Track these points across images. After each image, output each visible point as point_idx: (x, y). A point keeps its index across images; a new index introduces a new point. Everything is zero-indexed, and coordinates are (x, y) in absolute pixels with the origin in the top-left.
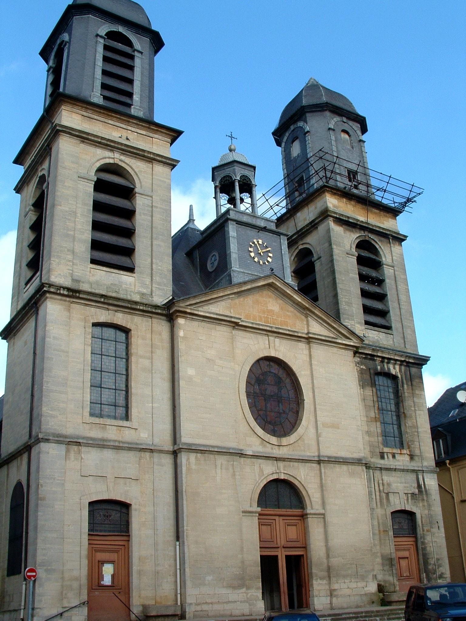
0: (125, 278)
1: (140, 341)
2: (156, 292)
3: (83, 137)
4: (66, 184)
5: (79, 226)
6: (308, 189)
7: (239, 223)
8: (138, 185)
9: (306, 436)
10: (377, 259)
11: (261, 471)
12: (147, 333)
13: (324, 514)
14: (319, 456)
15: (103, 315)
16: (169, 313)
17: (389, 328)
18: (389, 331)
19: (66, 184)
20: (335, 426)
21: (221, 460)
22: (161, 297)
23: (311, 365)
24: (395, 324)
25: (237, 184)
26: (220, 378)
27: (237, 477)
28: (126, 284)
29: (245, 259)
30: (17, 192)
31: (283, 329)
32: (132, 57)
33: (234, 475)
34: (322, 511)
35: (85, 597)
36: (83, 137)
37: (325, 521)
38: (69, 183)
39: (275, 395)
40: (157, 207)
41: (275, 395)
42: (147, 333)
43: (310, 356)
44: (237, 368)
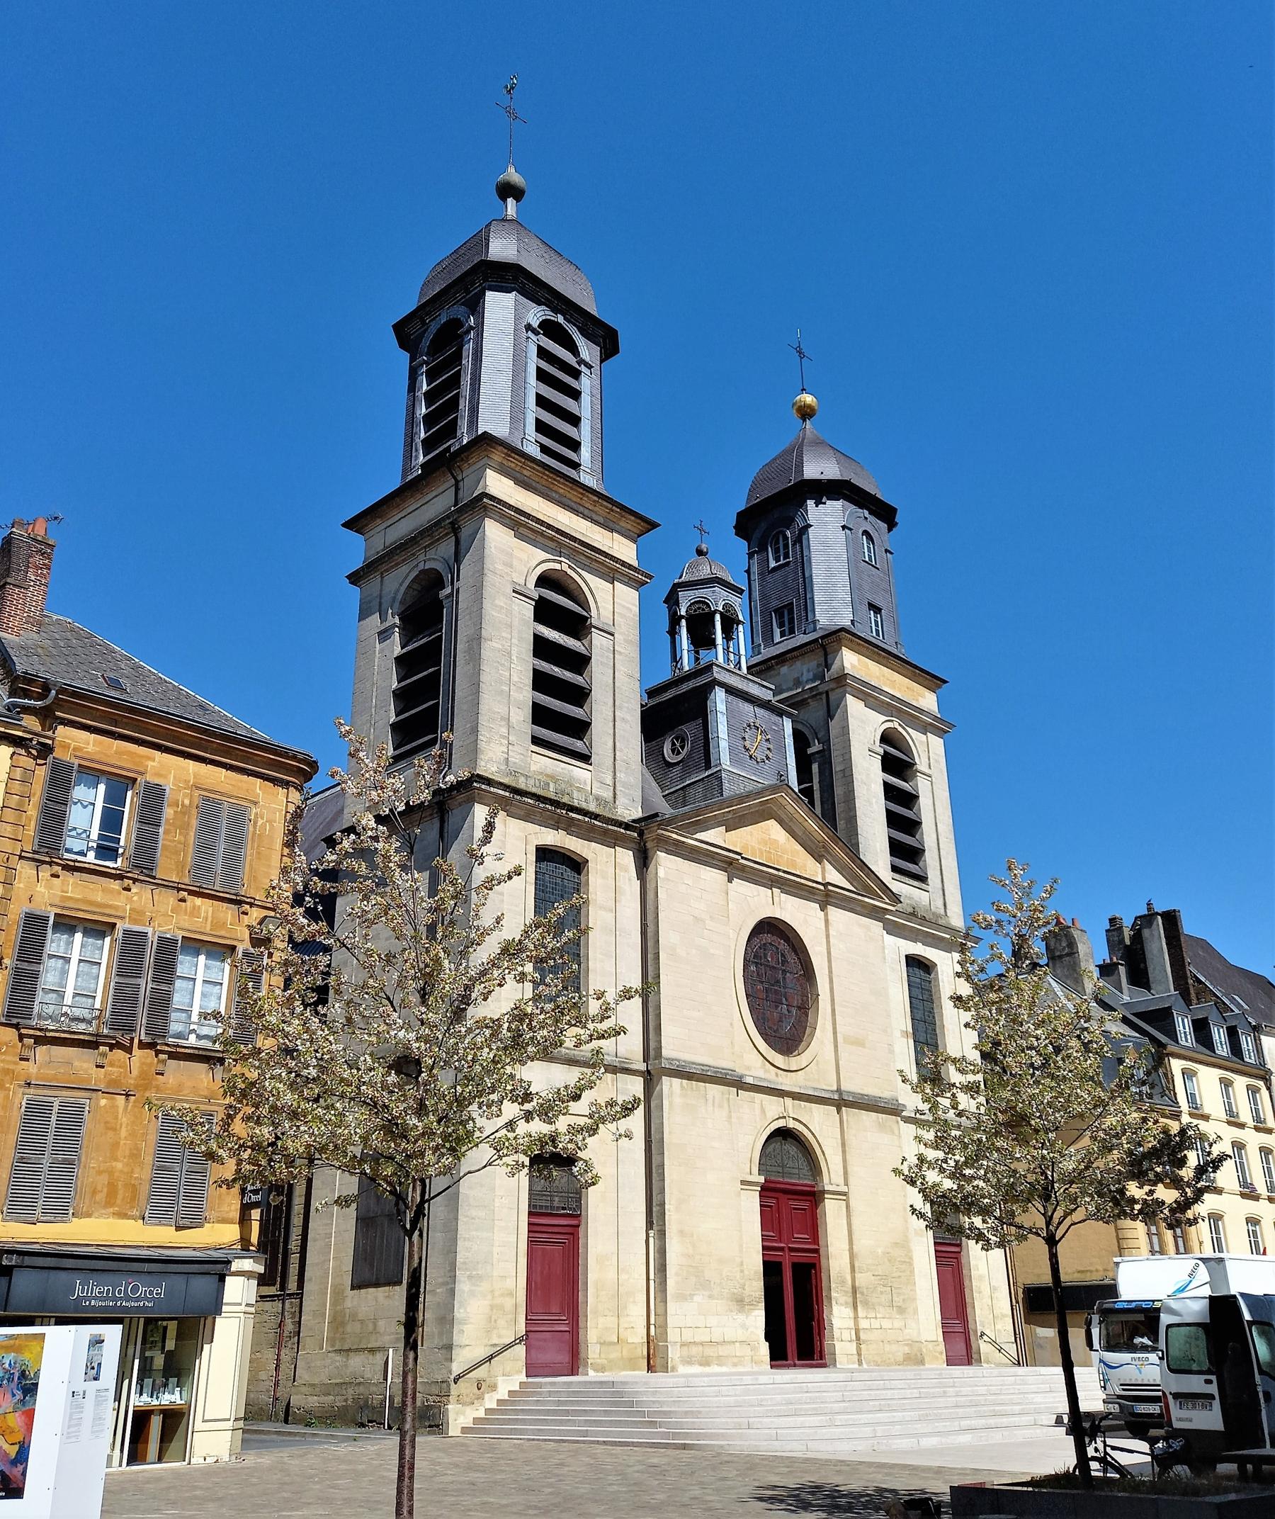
0: (578, 772)
1: (600, 881)
2: (621, 800)
3: (521, 524)
4: (497, 602)
5: (515, 678)
6: (990, 1196)
7: (730, 690)
8: (594, 613)
9: (817, 1064)
10: (50, 931)
11: (763, 1111)
12: (610, 870)
13: (845, 1194)
14: (839, 1091)
15: (551, 837)
16: (642, 839)
17: (922, 879)
18: (924, 886)
19: (497, 602)
20: (860, 1043)
21: (714, 1090)
22: (630, 810)
23: (828, 936)
24: (933, 875)
25: (718, 617)
26: (712, 951)
27: (733, 1120)
28: (581, 782)
29: (742, 752)
30: (352, 583)
31: (112, 766)
32: (576, 374)
33: (730, 1117)
34: (845, 1189)
35: (521, 1328)
36: (521, 524)
37: (848, 1207)
38: (500, 602)
39: (779, 981)
40: (620, 653)
41: (779, 981)
42: (610, 870)
43: (827, 921)
44: (732, 935)
